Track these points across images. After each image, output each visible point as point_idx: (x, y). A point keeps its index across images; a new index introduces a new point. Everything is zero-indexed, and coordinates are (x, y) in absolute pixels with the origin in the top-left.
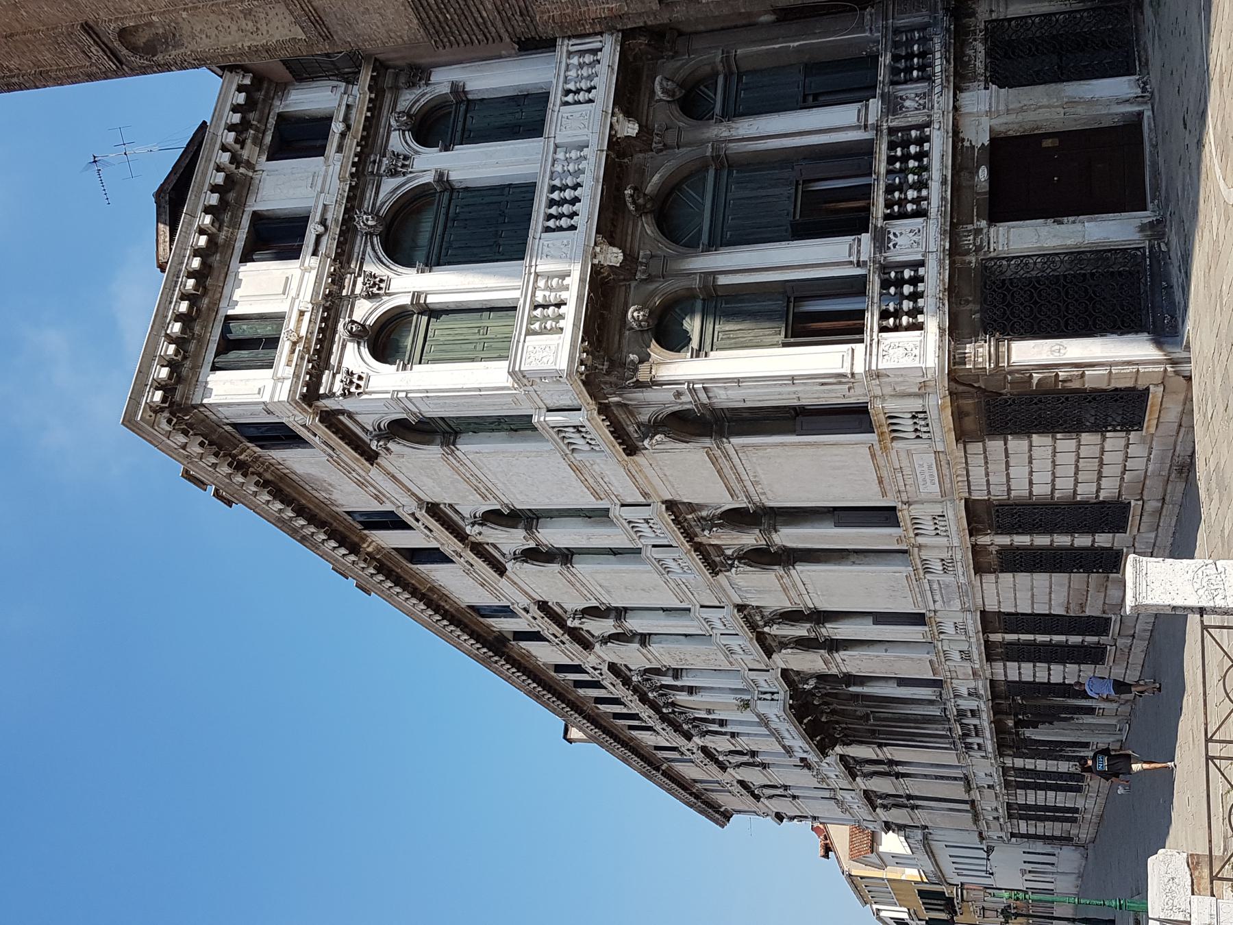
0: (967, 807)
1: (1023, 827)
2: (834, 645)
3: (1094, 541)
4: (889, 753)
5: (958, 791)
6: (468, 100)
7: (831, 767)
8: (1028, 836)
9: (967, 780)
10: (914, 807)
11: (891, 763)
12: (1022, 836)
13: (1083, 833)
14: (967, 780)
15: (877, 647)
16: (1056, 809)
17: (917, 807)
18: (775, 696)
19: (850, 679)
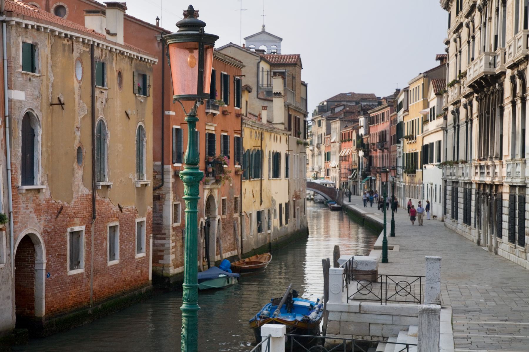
0: (456, 159)
1: (449, 188)
2: (514, 104)
3: (505, 207)
4: (476, 122)
5: (462, 157)
6: (270, 252)
7: (468, 90)
8: (445, 190)
9: (465, 162)
10: (454, 127)
11: (472, 121)
12: (445, 187)
13: (449, 220)
14: (465, 162)
15: (5, 157)
16: (457, 208)
17: (469, 45)
18: (492, 66)
19: (502, 109)
